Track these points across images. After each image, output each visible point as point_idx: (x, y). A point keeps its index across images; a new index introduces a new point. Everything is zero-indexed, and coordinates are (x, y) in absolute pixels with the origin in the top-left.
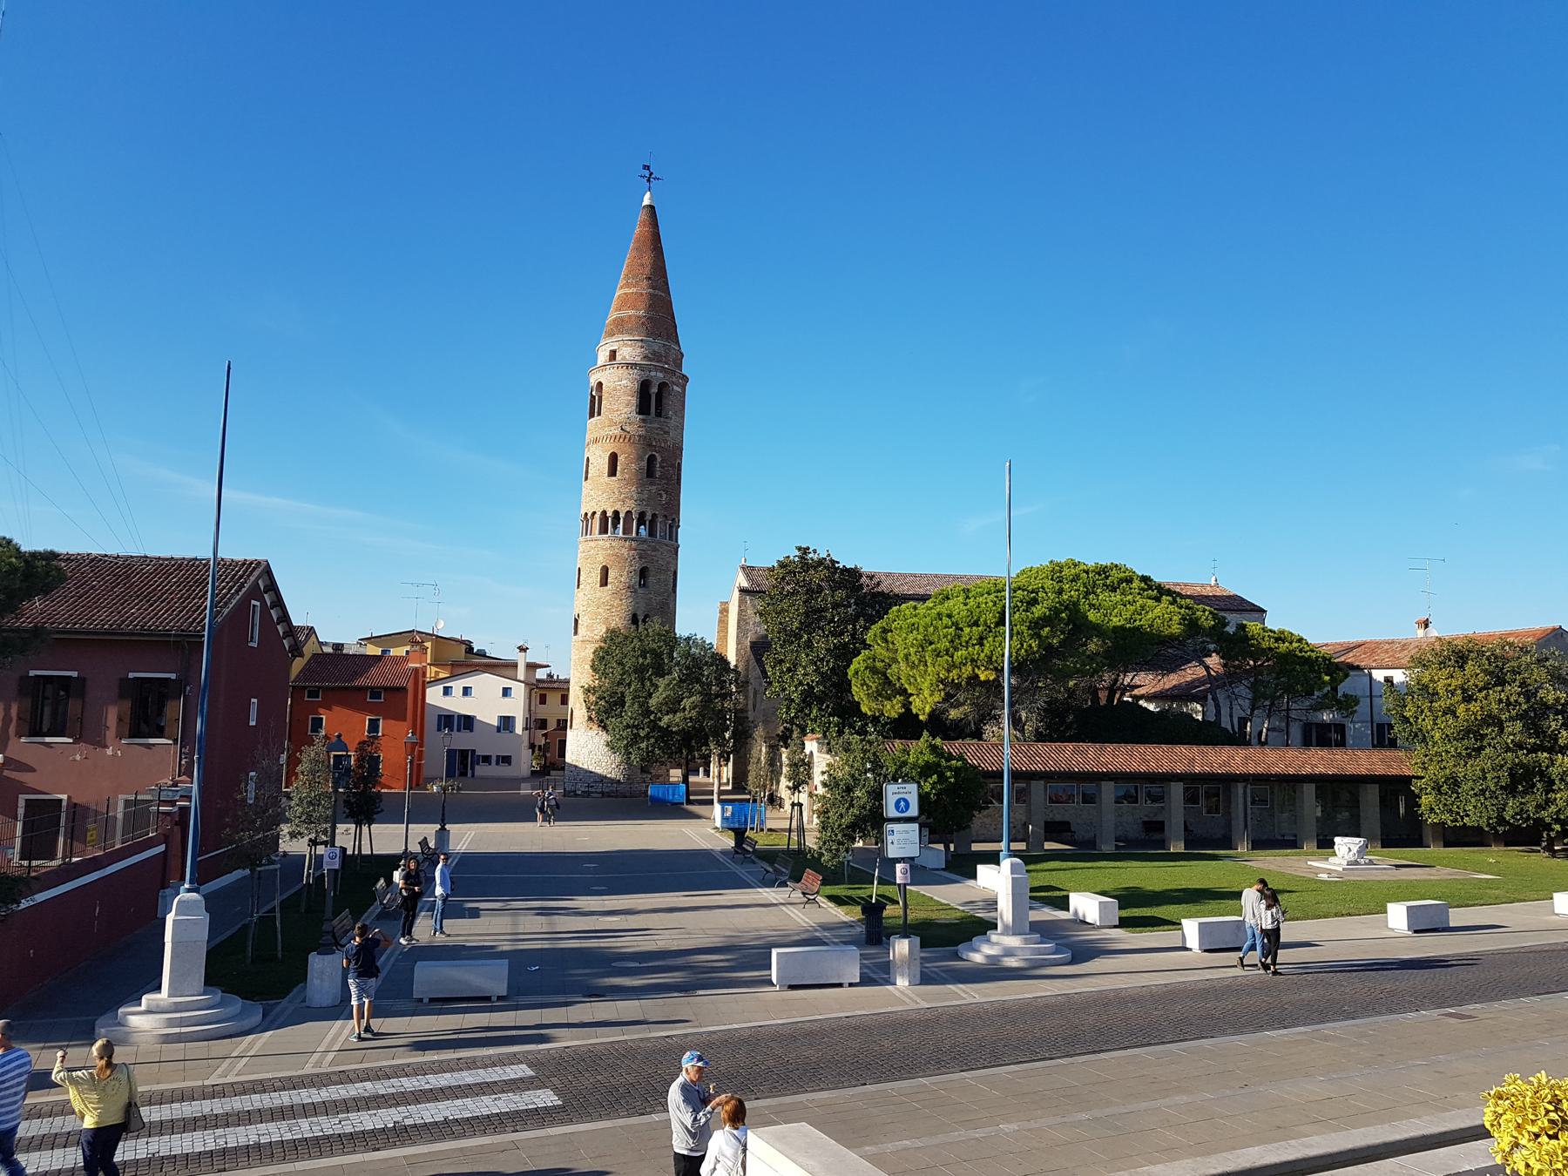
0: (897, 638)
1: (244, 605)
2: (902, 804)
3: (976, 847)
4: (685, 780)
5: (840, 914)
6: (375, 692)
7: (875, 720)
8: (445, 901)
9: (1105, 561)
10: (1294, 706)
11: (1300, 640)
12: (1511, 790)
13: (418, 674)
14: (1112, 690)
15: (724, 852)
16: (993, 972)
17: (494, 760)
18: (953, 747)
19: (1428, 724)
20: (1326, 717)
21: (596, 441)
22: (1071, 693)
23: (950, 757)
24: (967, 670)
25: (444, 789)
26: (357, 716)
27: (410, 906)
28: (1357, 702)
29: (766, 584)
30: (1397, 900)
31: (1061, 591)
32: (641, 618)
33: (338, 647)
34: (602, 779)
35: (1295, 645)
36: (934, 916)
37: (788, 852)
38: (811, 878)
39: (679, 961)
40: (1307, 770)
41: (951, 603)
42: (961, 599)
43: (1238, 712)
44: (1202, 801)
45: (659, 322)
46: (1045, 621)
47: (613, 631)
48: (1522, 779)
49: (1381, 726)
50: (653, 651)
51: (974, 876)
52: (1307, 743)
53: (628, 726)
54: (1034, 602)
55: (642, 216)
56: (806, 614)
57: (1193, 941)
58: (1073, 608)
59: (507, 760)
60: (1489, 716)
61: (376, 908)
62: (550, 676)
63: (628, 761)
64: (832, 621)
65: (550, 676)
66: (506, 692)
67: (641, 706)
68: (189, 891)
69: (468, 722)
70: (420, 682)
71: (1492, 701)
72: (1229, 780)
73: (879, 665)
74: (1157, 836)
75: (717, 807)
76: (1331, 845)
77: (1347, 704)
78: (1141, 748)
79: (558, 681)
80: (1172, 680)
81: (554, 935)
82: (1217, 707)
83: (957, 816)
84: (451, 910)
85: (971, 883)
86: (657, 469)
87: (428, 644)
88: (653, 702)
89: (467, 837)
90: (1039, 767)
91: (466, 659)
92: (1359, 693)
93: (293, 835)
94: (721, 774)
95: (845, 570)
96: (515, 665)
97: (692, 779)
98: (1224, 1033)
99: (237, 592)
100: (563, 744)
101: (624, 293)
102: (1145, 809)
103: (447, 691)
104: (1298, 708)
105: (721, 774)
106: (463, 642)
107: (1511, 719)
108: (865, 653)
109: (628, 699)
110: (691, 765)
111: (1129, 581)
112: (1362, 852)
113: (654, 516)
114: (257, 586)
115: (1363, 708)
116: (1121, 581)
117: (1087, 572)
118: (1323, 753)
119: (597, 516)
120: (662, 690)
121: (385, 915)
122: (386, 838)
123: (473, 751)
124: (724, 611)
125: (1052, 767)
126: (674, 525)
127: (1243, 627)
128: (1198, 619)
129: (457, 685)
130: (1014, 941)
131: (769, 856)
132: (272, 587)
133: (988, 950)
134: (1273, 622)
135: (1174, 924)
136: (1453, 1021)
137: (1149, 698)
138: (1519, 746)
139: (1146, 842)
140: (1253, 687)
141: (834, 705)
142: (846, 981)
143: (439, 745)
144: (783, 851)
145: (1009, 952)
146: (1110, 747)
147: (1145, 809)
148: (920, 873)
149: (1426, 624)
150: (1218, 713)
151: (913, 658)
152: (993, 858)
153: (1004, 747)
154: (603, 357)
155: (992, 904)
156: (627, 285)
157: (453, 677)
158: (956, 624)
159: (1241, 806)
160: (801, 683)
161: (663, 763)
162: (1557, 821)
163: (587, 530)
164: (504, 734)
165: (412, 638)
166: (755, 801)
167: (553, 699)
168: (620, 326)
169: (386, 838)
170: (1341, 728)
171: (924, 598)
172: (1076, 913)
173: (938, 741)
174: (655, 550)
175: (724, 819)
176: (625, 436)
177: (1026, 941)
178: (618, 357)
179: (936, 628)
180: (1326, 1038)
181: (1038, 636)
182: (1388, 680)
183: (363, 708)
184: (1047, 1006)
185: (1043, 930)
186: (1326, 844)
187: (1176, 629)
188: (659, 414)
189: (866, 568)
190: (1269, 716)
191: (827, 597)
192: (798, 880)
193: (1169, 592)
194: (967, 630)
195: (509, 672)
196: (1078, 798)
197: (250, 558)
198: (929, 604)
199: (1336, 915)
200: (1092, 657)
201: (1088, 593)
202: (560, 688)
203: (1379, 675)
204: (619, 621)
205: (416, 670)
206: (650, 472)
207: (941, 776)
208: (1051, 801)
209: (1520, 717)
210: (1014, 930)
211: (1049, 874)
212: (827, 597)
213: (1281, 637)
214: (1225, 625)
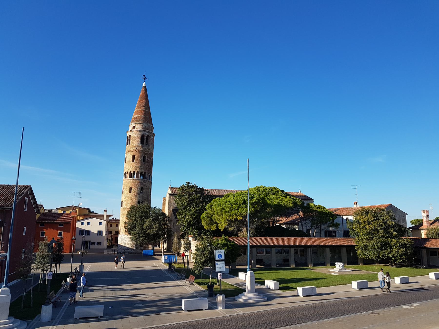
0: (214, 208)
1: (23, 199)
2: (220, 256)
3: (237, 267)
4: (153, 249)
5: (200, 288)
6: (61, 224)
7: (208, 231)
8: (83, 287)
9: (271, 186)
10: (322, 226)
11: (324, 208)
12: (381, 249)
13: (74, 219)
14: (274, 222)
15: (165, 270)
16: (246, 304)
17: (96, 244)
18: (231, 239)
19: (359, 231)
20: (331, 229)
21: (129, 151)
22: (262, 223)
23: (230, 242)
24: (234, 217)
25: (82, 253)
26: (55, 231)
27: (74, 288)
28: (339, 225)
29: (177, 192)
30: (354, 280)
31: (260, 195)
32: (141, 202)
33: (50, 211)
34: (129, 249)
35: (323, 209)
36: (227, 288)
37: (184, 270)
38: (192, 277)
39: (155, 304)
40: (327, 244)
41: (229, 198)
42: (232, 197)
43: (308, 228)
44: (299, 253)
45: (147, 118)
46: (256, 203)
47: (133, 206)
48: (384, 246)
49: (345, 231)
50: (144, 212)
51: (238, 276)
52: (326, 236)
53: (137, 233)
54: (253, 198)
55: (142, 89)
56: (189, 201)
57: (300, 294)
58: (263, 199)
59: (100, 243)
60: (375, 228)
61: (61, 290)
62: (113, 218)
63: (137, 244)
64: (196, 203)
65: (113, 218)
66: (100, 223)
67: (141, 227)
68: (5, 287)
69: (88, 232)
70: (75, 221)
71: (375, 224)
72: (306, 247)
73: (210, 215)
74: (287, 263)
75: (163, 257)
76: (335, 265)
77: (337, 225)
78: (283, 238)
79: (116, 220)
80: (290, 219)
81: (117, 297)
82: (302, 226)
83: (235, 258)
84: (85, 290)
85: (237, 278)
86: (146, 160)
87: (77, 210)
88: (145, 226)
89: (89, 267)
90: (255, 244)
91: (88, 214)
92: (339, 222)
93: (37, 268)
94: (163, 246)
95: (200, 189)
96: (103, 216)
97: (155, 248)
98: (312, 321)
99: (21, 195)
100: (117, 239)
101: (137, 110)
102: (284, 255)
103: (82, 223)
104: (323, 227)
105: (163, 246)
106: (87, 209)
107: (381, 229)
108: (205, 212)
109: (137, 225)
110: (155, 244)
111: (278, 192)
112: (343, 266)
113: (145, 173)
114: (27, 193)
115: (341, 226)
116: (276, 192)
117: (266, 189)
118: (331, 239)
119: (129, 173)
120: (147, 223)
121: (65, 292)
122: (65, 268)
123: (90, 241)
124: (164, 200)
125: (258, 244)
126: (151, 176)
127: (309, 204)
128: (297, 202)
129: (85, 222)
130: (251, 295)
131: (179, 271)
132: (32, 193)
133: (244, 298)
134: (316, 203)
135: (294, 288)
136: (373, 315)
137: (283, 224)
138: (383, 236)
139: (284, 265)
140: (311, 221)
141: (197, 228)
142: (204, 308)
143: (80, 239)
144: (182, 269)
145: (250, 298)
146: (274, 238)
147: (284, 255)
148: (225, 276)
149: (356, 203)
150: (303, 228)
151: (219, 213)
152: (245, 271)
153: (246, 237)
154: (131, 128)
155: (244, 284)
156: (138, 108)
157: (84, 219)
158: (231, 204)
159: (310, 254)
160: (187, 221)
161: (147, 244)
162: (393, 257)
163: (125, 177)
164: (99, 236)
165: (72, 208)
166: (174, 254)
167: (114, 225)
168: (136, 119)
169: (65, 268)
170: (335, 232)
171: (221, 196)
172: (267, 286)
173: (227, 237)
174: (145, 182)
175: (165, 260)
176: (137, 150)
177: (255, 295)
178: (135, 128)
179: (225, 205)
180: (340, 321)
181: (254, 207)
182: (347, 219)
183: (57, 229)
184: (262, 314)
185: (259, 291)
186: (333, 264)
187: (291, 205)
188: (147, 144)
189: (205, 188)
190: (316, 229)
191: (194, 196)
192: (188, 278)
193: (289, 195)
194: (234, 206)
195: (101, 218)
196: (265, 253)
197: (25, 185)
198: (223, 198)
199: (338, 285)
200: (268, 213)
201: (267, 195)
202: (117, 223)
203: (345, 217)
204: (134, 203)
205: (74, 217)
206: (144, 161)
207: (228, 247)
208: (258, 254)
209: (383, 229)
210: (251, 292)
211: (261, 275)
212: (194, 196)
213: (319, 207)
214: (304, 204)
